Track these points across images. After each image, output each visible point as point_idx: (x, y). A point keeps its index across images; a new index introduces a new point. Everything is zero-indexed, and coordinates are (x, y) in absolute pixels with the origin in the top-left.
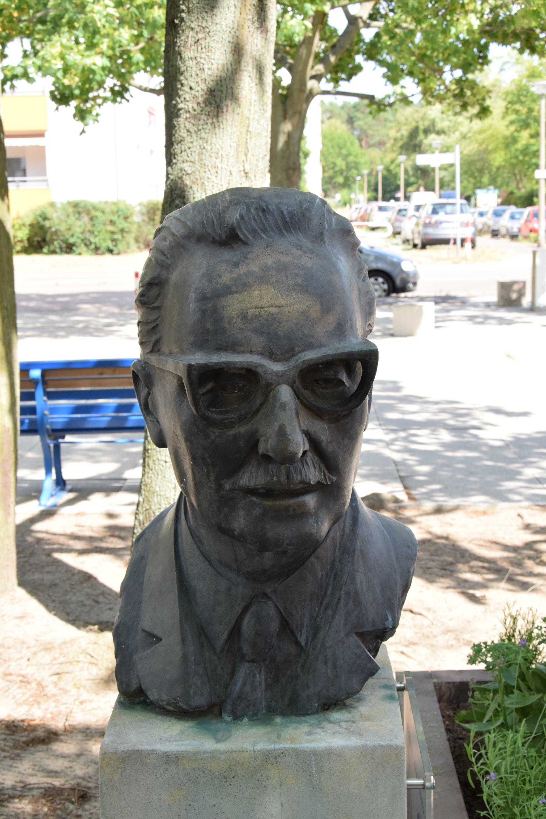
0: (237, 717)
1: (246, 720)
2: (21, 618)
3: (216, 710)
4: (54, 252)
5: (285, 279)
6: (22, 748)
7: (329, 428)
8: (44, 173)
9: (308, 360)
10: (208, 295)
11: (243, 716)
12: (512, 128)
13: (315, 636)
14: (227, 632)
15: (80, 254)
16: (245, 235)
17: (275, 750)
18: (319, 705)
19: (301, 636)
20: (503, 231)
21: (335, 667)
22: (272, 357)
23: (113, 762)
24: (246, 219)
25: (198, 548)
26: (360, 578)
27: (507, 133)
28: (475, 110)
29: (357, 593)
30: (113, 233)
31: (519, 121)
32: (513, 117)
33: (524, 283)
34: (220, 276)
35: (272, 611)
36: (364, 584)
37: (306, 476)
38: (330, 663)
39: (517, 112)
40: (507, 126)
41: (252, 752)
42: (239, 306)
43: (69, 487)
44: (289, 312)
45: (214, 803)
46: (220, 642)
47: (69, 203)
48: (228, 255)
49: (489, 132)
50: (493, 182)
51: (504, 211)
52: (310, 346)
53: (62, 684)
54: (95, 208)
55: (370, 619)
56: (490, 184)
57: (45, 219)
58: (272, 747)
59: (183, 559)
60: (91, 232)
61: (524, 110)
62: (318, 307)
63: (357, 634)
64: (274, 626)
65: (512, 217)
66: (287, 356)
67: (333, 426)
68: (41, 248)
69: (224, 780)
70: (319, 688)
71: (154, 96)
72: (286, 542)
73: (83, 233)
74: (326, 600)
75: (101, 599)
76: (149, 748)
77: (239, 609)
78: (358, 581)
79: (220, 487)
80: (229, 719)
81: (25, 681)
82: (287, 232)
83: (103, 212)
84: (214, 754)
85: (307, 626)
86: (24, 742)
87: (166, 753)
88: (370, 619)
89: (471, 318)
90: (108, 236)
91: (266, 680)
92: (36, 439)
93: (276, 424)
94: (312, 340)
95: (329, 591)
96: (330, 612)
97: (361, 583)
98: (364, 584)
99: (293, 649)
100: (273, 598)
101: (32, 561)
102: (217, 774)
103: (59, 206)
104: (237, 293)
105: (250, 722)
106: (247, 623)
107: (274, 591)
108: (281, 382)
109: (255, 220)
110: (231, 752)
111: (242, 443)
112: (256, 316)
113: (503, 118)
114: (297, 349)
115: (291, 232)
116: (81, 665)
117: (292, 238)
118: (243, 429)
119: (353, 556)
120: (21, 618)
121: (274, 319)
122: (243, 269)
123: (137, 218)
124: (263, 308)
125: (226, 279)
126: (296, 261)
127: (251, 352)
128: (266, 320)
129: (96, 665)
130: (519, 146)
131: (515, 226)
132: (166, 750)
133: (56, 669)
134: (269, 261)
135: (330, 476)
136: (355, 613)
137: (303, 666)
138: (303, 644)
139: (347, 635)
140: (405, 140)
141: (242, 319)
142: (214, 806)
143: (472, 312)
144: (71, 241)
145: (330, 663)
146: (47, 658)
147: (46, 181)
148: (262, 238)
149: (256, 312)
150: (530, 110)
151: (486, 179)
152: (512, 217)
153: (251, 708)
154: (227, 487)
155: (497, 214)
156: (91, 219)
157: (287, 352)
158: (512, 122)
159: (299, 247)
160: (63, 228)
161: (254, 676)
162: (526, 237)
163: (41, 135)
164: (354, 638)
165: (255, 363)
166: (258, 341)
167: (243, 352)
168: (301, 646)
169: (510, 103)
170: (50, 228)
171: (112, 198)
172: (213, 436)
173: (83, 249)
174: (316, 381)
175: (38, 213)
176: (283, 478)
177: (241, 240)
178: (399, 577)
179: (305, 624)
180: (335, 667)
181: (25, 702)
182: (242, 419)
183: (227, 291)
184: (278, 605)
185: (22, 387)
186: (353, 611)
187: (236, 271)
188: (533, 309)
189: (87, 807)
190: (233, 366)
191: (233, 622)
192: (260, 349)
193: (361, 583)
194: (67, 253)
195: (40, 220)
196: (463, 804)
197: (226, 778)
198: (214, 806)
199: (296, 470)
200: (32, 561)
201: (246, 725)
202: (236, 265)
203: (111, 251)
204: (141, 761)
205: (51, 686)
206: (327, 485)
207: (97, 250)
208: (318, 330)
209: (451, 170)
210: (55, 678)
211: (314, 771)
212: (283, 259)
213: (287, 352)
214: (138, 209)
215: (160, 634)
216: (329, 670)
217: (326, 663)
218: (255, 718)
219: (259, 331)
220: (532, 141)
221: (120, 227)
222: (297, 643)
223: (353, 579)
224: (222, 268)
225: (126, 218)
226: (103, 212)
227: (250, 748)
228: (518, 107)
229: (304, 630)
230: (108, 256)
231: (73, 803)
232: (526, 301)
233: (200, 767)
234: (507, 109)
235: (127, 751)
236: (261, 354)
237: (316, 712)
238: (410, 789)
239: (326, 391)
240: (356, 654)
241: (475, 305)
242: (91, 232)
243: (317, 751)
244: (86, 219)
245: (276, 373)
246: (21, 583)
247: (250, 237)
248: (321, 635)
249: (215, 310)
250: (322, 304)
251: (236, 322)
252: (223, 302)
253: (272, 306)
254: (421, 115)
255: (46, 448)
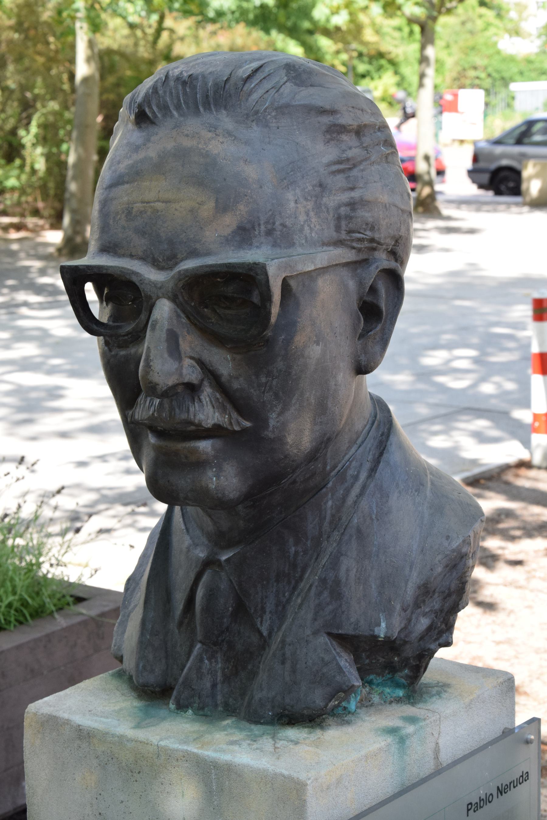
0: (181, 707)
7: (233, 359)
9: (184, 270)
11: (187, 707)
16: (154, 113)
18: (273, 715)
19: (261, 623)
21: (294, 671)
22: (156, 264)
23: (33, 724)
24: (161, 92)
29: (337, 582)
36: (353, 574)
37: (195, 416)
38: (288, 665)
41: (156, 747)
44: (176, 210)
52: (194, 254)
55: (352, 620)
62: (211, 204)
67: (238, 357)
69: (130, 774)
70: (273, 693)
76: (66, 716)
78: (343, 568)
82: (205, 109)
85: (271, 612)
87: (79, 726)
88: (352, 620)
91: (223, 669)
94: (198, 246)
97: (348, 570)
98: (353, 574)
99: (255, 639)
102: (124, 764)
105: (195, 717)
108: (161, 295)
109: (171, 93)
112: (141, 212)
114: (179, 256)
115: (210, 109)
117: (208, 117)
124: (149, 202)
126: (200, 146)
127: (131, 256)
132: (80, 723)
135: (240, 419)
136: (330, 607)
138: (265, 633)
139: (315, 633)
142: (122, 802)
145: (288, 665)
148: (172, 116)
153: (196, 699)
159: (213, 128)
164: (323, 639)
165: (128, 269)
167: (123, 256)
178: (415, 574)
179: (268, 610)
180: (294, 671)
184: (232, 578)
186: (328, 604)
190: (104, 271)
191: (188, 590)
192: (140, 253)
193: (348, 570)
197: (132, 772)
198: (122, 802)
201: (187, 718)
204: (58, 730)
206: (235, 432)
208: (207, 233)
211: (214, 788)
216: (286, 673)
217: (283, 663)
218: (201, 713)
219: (141, 232)
227: (155, 742)
233: (109, 751)
235: (46, 714)
236: (143, 259)
237: (271, 723)
239: (228, 312)
240: (323, 660)
243: (217, 763)
245: (154, 284)
247: (159, 115)
250: (217, 201)
251: (120, 219)
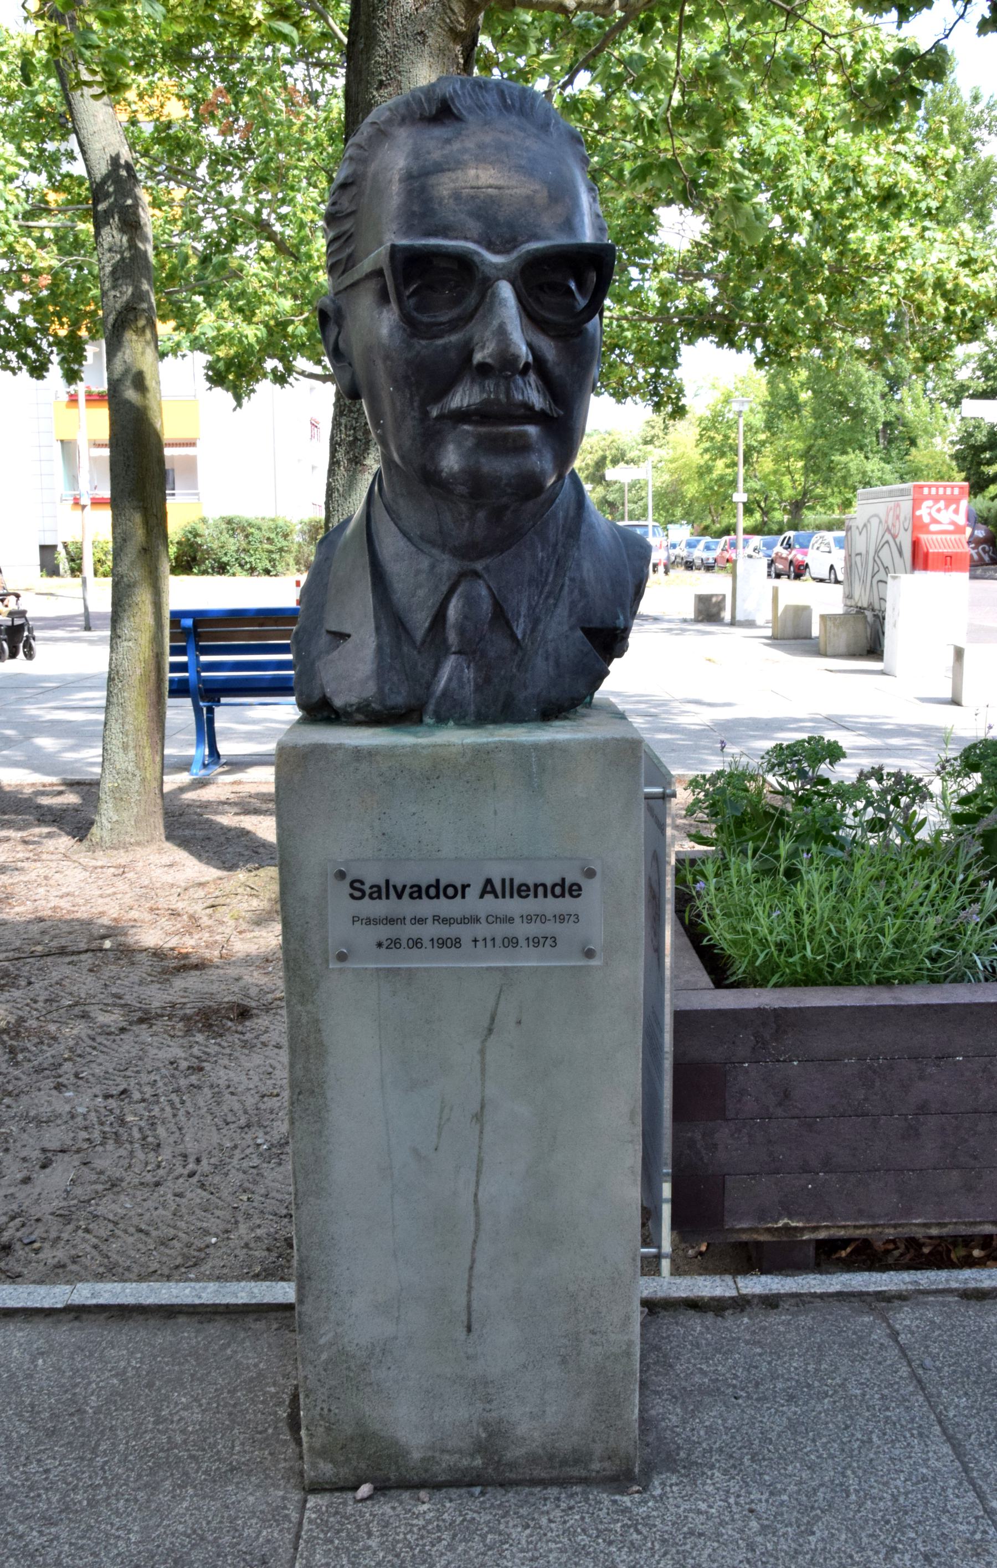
1: (451, 723)
2: (171, 866)
3: (415, 716)
4: (205, 572)
5: (506, 160)
6: (172, 973)
7: (556, 347)
8: (195, 486)
10: (415, 173)
12: (707, 456)
13: (533, 630)
14: (429, 620)
15: (234, 575)
17: (487, 744)
20: (698, 562)
22: (491, 247)
25: (396, 524)
26: (586, 565)
27: (702, 462)
28: (669, 408)
30: (270, 552)
31: (714, 448)
32: (708, 444)
33: (724, 596)
34: (429, 153)
35: (484, 592)
39: (712, 439)
40: (702, 454)
42: (452, 185)
43: (223, 760)
45: (414, 810)
46: (419, 634)
47: (223, 518)
48: (439, 132)
49: (680, 462)
50: (687, 515)
51: (698, 541)
52: (534, 237)
53: (218, 916)
54: (250, 525)
56: (682, 519)
57: (196, 535)
58: (485, 740)
59: (376, 543)
60: (246, 551)
61: (719, 438)
62: (545, 194)
63: (583, 629)
64: (486, 606)
65: (707, 548)
66: (508, 246)
68: (191, 569)
71: (318, 384)
72: (504, 482)
73: (237, 551)
74: (547, 589)
75: (261, 850)
77: (444, 589)
79: (425, 414)
80: (431, 721)
81: (175, 914)
83: (259, 529)
84: (414, 749)
86: (174, 968)
89: (670, 630)
90: (265, 555)
91: (475, 679)
92: (187, 702)
93: (495, 323)
94: (538, 230)
95: (550, 579)
96: (551, 601)
99: (507, 645)
100: (486, 576)
101: (182, 820)
103: (211, 522)
104: (449, 170)
106: (453, 612)
107: (487, 568)
110: (434, 746)
111: (453, 355)
113: (697, 446)
116: (239, 897)
118: (454, 338)
119: (578, 540)
120: (171, 866)
121: (493, 202)
122: (456, 146)
123: (297, 538)
125: (436, 155)
128: (483, 202)
129: (257, 896)
130: (715, 475)
131: (710, 556)
133: (210, 902)
134: (488, 139)
137: (519, 666)
138: (520, 637)
140: (591, 470)
141: (456, 199)
143: (666, 625)
144: (225, 559)
146: (201, 893)
147: (197, 494)
149: (472, 192)
150: (726, 437)
151: (679, 512)
152: (707, 548)
154: (435, 413)
155: (691, 545)
156: (247, 536)
157: (507, 242)
158: (706, 450)
160: (215, 545)
161: (462, 671)
162: (723, 568)
163: (192, 444)
166: (474, 227)
168: (518, 640)
169: (704, 429)
170: (201, 545)
171: (270, 514)
172: (418, 347)
173: (237, 569)
174: (541, 288)
175: (189, 528)
176: (502, 397)
177: (453, 114)
181: (176, 933)
182: (454, 325)
183: (439, 168)
185: (171, 640)
187: (448, 147)
188: (733, 623)
189: (247, 1023)
194: (219, 573)
195: (190, 536)
196: (690, 945)
199: (517, 388)
200: (182, 820)
202: (448, 141)
203: (267, 572)
205: (205, 919)
206: (552, 417)
207: (252, 570)
209: (641, 503)
210: (210, 911)
212: (504, 138)
213: (507, 242)
214: (298, 527)
215: (347, 631)
220: (729, 471)
221: (279, 545)
222: (513, 636)
223: (579, 566)
224: (431, 144)
225: (285, 536)
226: (259, 529)
228: (712, 434)
229: (522, 620)
230: (266, 578)
231: (231, 1020)
232: (727, 615)
234: (701, 436)
238: (649, 797)
241: (670, 621)
242: (246, 551)
244: (241, 537)
245: (495, 266)
246: (169, 838)
248: (541, 627)
249: (423, 189)
252: (433, 180)
253: (491, 187)
254: (607, 443)
255: (198, 710)
